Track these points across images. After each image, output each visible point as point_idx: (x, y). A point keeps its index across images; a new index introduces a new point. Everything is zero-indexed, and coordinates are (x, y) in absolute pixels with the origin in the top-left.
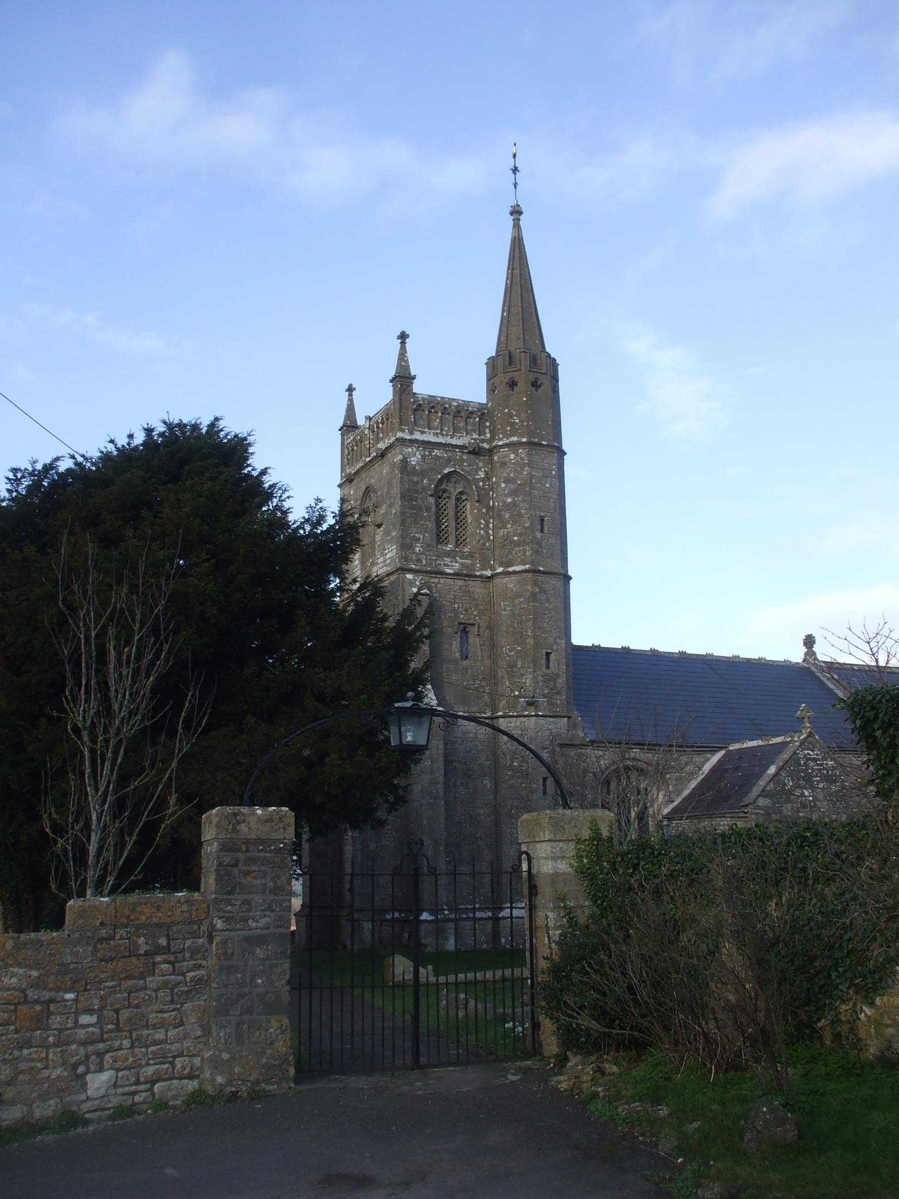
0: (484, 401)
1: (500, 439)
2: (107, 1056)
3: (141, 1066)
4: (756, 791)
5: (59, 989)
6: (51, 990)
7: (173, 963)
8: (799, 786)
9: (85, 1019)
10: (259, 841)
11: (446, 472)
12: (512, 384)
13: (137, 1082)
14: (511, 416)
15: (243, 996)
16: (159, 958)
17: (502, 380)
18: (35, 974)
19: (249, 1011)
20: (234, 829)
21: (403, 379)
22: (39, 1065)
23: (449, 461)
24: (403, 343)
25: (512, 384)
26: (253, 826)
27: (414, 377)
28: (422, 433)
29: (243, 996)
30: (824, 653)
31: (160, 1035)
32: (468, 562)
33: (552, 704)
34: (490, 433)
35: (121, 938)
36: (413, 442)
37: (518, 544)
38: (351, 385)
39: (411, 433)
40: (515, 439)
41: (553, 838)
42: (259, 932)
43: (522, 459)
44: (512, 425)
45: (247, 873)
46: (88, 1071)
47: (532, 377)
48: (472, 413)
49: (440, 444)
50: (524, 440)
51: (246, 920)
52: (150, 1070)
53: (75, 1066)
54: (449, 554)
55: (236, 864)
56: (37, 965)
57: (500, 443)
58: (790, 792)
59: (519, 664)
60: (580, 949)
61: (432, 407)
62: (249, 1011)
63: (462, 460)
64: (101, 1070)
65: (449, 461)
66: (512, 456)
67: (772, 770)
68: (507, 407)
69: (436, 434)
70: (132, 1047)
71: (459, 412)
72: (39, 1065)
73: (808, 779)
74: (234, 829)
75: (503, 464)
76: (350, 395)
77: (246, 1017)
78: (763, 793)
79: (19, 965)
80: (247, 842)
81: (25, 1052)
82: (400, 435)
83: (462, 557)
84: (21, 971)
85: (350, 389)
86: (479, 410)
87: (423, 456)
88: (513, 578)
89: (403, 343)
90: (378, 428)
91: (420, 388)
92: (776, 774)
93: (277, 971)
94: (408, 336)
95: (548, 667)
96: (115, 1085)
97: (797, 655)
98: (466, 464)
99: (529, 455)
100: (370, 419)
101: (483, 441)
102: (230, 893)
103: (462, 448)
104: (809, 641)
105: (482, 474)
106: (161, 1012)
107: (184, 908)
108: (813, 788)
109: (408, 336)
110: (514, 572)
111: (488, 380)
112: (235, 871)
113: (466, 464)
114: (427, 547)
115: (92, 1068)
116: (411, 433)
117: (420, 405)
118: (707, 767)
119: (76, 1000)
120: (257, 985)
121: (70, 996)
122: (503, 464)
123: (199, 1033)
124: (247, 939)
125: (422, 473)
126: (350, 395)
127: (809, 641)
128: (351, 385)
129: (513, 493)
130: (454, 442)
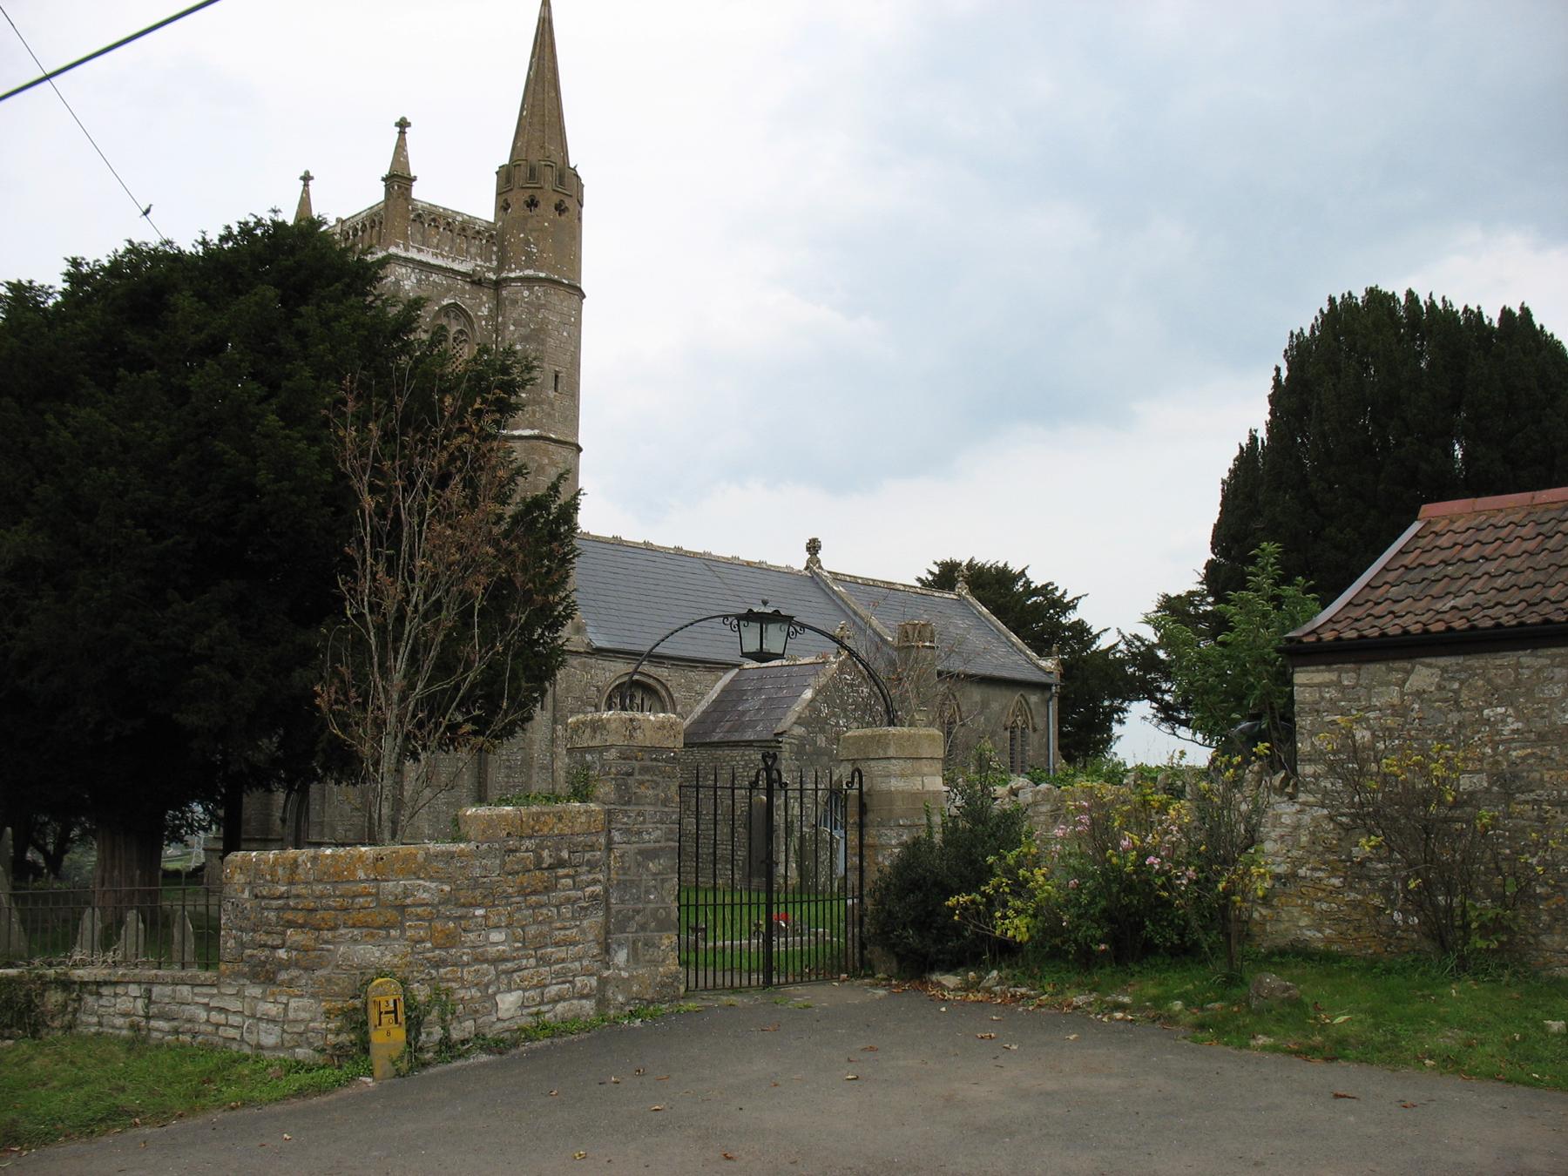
0: (492, 220)
1: (511, 270)
2: (515, 975)
3: (545, 986)
4: (791, 717)
5: (471, 905)
6: (463, 906)
7: (572, 877)
8: (835, 715)
9: (496, 936)
10: (654, 749)
11: (445, 303)
12: (532, 203)
13: (542, 1003)
14: (528, 243)
15: (638, 912)
16: (561, 872)
17: (518, 198)
18: (447, 888)
19: (643, 927)
20: (631, 736)
21: (399, 180)
22: (454, 985)
23: (449, 289)
24: (402, 133)
25: (532, 203)
26: (648, 734)
27: (415, 179)
28: (420, 250)
29: (638, 912)
30: (830, 561)
31: (561, 953)
34: (498, 260)
35: (527, 850)
36: (407, 260)
38: (307, 173)
39: (407, 250)
40: (530, 272)
42: (652, 845)
43: (538, 298)
44: (529, 254)
45: (642, 783)
46: (498, 991)
47: (556, 198)
48: (478, 232)
49: (439, 268)
50: (542, 275)
51: (639, 833)
52: (553, 990)
53: (487, 986)
55: (631, 774)
56: (450, 879)
57: (512, 275)
61: (434, 220)
62: (643, 927)
64: (510, 990)
65: (449, 289)
66: (526, 293)
67: (808, 694)
68: (523, 231)
69: (435, 255)
70: (538, 965)
71: (464, 229)
72: (454, 985)
74: (631, 736)
75: (514, 302)
76: (306, 185)
77: (641, 934)
78: (799, 721)
79: (432, 879)
80: (643, 749)
81: (442, 971)
82: (393, 250)
84: (433, 885)
85: (307, 178)
86: (487, 230)
87: (419, 281)
89: (402, 133)
90: (355, 235)
91: (419, 193)
92: (813, 700)
93: (667, 886)
94: (409, 125)
96: (523, 1006)
97: (799, 561)
99: (545, 293)
100: (343, 222)
101: (489, 269)
102: (628, 803)
103: (464, 275)
104: (813, 547)
105: (485, 311)
106: (565, 928)
107: (583, 819)
109: (409, 125)
110: (521, 438)
111: (498, 194)
112: (631, 781)
115: (503, 987)
116: (407, 250)
117: (419, 216)
118: (713, 694)
119: (485, 917)
120: (649, 901)
121: (480, 912)
122: (514, 302)
123: (596, 951)
124: (640, 852)
126: (306, 185)
127: (813, 547)
128: (307, 173)
129: (525, 339)
130: (456, 266)
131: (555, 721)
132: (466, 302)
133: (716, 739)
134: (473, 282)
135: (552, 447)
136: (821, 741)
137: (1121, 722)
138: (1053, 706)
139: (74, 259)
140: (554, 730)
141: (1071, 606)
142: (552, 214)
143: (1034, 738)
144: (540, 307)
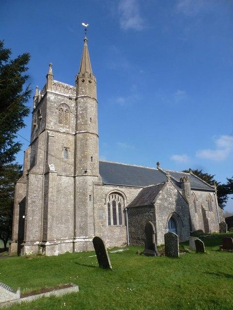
23: (63, 100)
32: (68, 130)
33: (92, 172)
37: (83, 125)
40: (83, 95)
41: (77, 190)
44: (83, 92)
47: (89, 79)
49: (60, 95)
54: (62, 127)
58: (166, 199)
59: (83, 160)
60: (7, 67)
63: (67, 101)
65: (63, 100)
73: (171, 195)
83: (66, 128)
87: (55, 98)
88: (82, 134)
95: (192, 189)
98: (68, 102)
103: (67, 97)
105: (73, 105)
108: (172, 198)
113: (68, 102)
114: (55, 124)
125: (55, 102)
129: (82, 110)
131: (94, 204)
132: (68, 103)
133: (137, 206)
134: (69, 99)
135: (90, 135)
136: (166, 204)
137: (226, 202)
138: (216, 195)
139: (83, 309)
140: (94, 206)
141: (212, 177)
142: (88, 83)
143: (213, 203)
144: (86, 103)
